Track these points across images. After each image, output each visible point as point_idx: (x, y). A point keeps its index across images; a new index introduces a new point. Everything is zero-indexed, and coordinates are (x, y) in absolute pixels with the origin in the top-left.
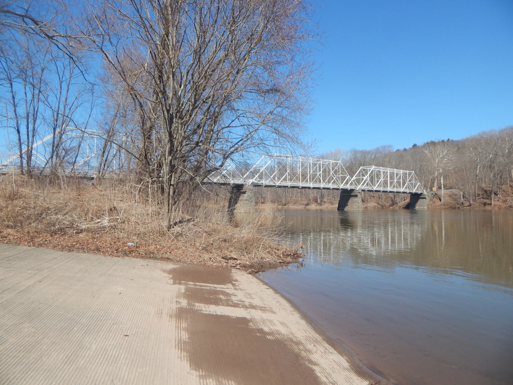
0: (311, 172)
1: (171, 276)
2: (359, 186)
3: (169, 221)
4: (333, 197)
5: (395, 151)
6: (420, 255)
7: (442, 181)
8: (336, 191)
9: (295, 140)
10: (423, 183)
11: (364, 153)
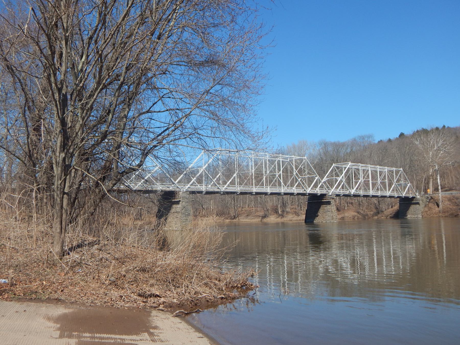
0: (268, 172)
1: (59, 326)
2: (333, 190)
3: (62, 246)
4: (298, 206)
5: (376, 142)
6: (416, 280)
7: (439, 180)
8: (302, 197)
9: (240, 128)
10: (415, 183)
11: (338, 146)
